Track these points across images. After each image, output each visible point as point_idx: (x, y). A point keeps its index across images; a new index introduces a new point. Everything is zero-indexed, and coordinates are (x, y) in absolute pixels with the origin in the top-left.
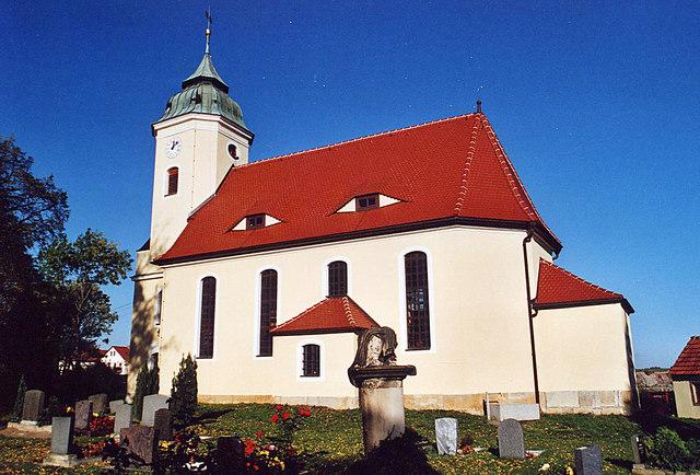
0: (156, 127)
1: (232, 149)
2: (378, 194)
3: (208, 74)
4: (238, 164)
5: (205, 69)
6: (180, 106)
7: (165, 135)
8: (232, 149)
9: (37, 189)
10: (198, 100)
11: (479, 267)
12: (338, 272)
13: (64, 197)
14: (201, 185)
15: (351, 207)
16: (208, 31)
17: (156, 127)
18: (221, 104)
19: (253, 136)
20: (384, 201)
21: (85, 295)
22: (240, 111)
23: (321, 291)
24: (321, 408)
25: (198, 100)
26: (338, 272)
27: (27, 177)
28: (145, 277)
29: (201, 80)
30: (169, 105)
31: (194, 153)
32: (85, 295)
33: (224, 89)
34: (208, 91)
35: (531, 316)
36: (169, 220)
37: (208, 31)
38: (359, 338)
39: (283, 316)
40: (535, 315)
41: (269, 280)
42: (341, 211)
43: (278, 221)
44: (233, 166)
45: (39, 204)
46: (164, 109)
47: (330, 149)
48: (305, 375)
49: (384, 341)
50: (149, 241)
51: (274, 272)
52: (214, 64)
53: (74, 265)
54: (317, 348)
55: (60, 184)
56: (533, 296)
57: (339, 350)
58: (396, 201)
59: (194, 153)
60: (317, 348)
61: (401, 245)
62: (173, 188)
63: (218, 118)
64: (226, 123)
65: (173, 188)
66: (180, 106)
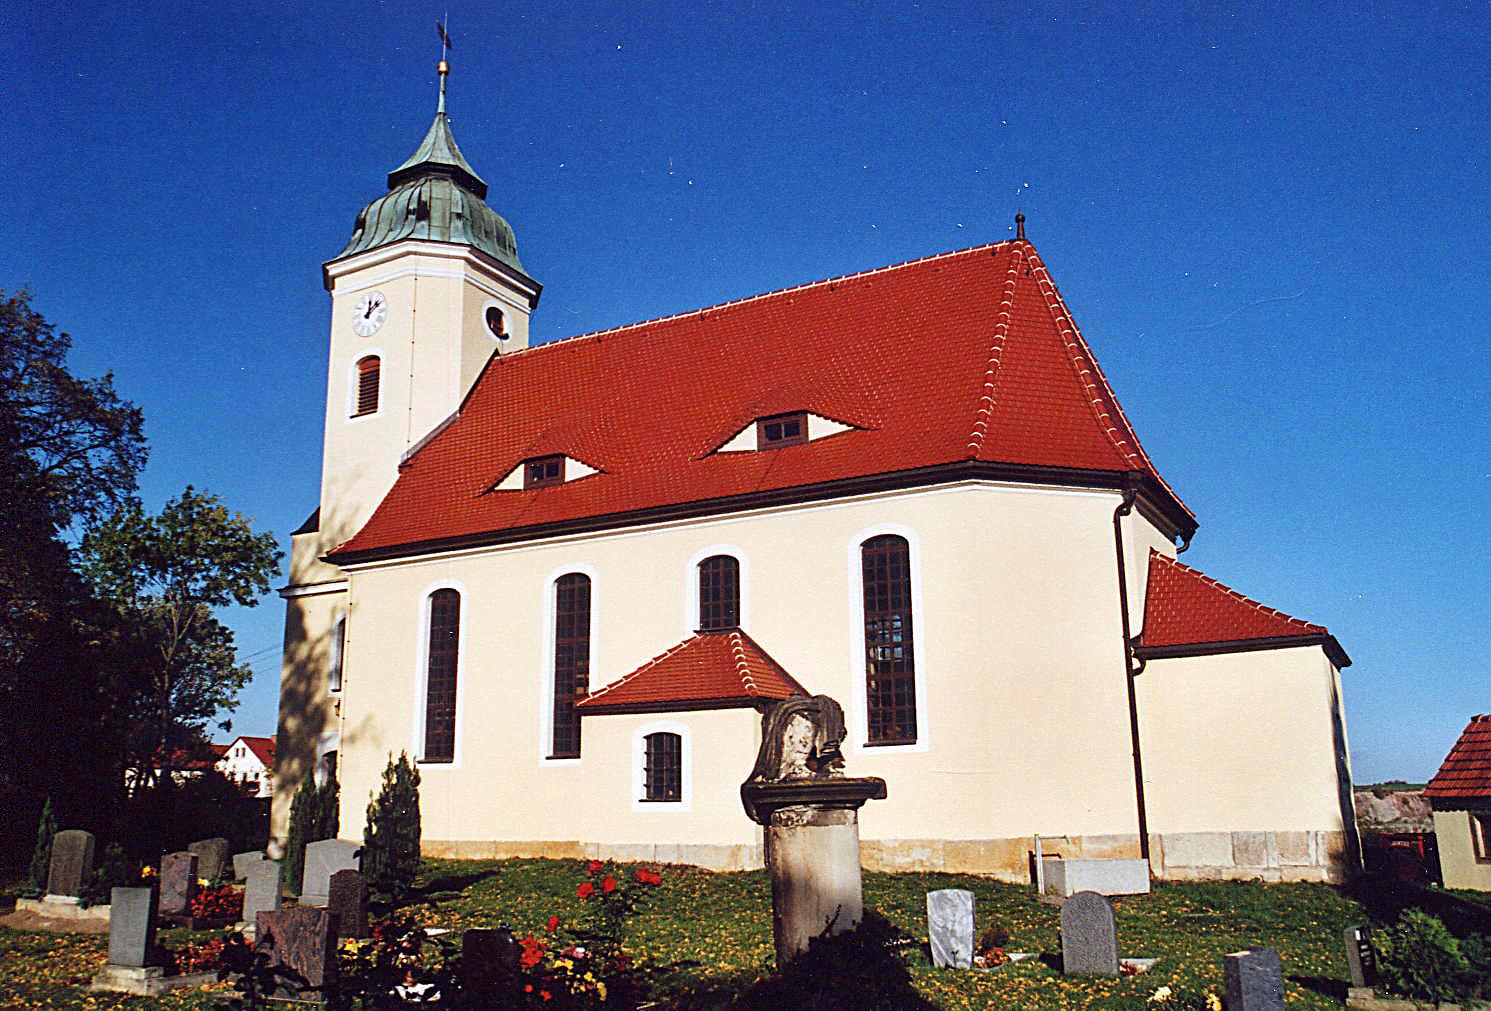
0: (333, 270)
1: (494, 317)
3: (444, 157)
4: (509, 348)
5: (436, 146)
6: (384, 227)
7: (352, 287)
8: (494, 317)
9: (80, 402)
10: (423, 212)
11: (1021, 573)
12: (720, 581)
13: (136, 418)
14: (428, 393)
15: (748, 440)
16: (443, 67)
17: (333, 270)
18: (471, 221)
20: (819, 428)
21: (181, 628)
22: (512, 237)
25: (423, 212)
26: (720, 581)
27: (59, 377)
28: (310, 590)
29: (428, 170)
30: (361, 224)
32: (181, 628)
33: (480, 191)
34: (444, 195)
35: (1132, 674)
37: (443, 67)
40: (1140, 671)
42: (726, 448)
44: (496, 353)
46: (347, 232)
55: (126, 393)
56: (1135, 630)
57: (722, 745)
58: (844, 428)
59: (414, 327)
61: (843, 527)
62: (368, 400)
63: (465, 252)
64: (482, 261)
65: (368, 400)
66: (384, 227)
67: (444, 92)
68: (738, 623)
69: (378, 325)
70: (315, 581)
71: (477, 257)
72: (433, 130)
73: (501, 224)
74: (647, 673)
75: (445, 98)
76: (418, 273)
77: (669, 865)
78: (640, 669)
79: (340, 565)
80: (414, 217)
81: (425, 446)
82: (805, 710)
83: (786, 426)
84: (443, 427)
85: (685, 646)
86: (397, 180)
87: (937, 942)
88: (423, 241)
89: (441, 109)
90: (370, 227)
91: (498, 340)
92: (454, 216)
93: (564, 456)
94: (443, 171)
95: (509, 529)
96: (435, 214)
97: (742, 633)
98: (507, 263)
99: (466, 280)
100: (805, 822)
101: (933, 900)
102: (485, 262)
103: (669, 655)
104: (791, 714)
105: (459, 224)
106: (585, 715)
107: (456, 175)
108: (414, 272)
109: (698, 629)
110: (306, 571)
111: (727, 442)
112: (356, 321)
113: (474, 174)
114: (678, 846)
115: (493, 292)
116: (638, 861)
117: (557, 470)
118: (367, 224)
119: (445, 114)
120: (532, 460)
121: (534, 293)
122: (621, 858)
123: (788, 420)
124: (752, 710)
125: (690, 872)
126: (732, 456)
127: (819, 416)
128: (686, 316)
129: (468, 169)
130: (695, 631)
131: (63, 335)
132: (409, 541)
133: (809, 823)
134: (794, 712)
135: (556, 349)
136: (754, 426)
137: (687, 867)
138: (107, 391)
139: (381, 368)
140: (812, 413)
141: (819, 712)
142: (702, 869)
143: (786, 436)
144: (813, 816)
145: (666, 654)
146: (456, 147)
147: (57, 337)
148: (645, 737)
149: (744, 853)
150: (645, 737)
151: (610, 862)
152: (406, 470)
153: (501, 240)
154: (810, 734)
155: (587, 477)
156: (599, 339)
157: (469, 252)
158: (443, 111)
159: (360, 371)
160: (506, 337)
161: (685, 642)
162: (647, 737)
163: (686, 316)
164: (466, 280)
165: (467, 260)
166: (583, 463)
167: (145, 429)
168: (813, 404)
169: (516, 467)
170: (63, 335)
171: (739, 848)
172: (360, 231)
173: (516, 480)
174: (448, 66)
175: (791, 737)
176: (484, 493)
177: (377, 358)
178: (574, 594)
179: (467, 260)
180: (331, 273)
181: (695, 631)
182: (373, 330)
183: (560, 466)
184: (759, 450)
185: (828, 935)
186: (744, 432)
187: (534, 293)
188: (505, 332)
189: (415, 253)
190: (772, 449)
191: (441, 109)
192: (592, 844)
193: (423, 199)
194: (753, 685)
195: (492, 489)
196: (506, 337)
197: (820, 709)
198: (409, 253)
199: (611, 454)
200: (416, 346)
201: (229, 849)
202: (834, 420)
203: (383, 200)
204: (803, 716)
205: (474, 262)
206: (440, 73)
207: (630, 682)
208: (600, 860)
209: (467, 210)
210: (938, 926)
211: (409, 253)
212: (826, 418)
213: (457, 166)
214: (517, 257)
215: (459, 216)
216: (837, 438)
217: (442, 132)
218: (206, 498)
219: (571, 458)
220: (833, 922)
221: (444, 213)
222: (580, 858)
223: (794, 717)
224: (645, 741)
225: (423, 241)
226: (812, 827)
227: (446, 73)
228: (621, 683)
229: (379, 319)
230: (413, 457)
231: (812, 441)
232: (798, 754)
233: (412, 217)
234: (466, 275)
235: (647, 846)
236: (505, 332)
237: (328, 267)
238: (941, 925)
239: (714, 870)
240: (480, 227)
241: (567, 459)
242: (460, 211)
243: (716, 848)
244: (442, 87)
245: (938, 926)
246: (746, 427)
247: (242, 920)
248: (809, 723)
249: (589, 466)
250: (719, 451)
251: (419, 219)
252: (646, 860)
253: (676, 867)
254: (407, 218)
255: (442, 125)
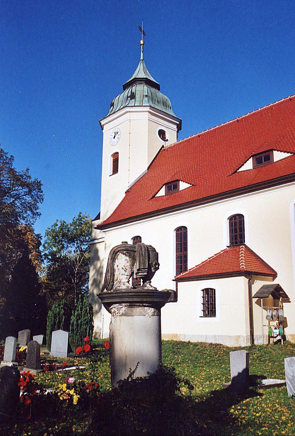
0: (103, 123)
1: (162, 134)
2: (272, 150)
4: (167, 144)
5: (140, 72)
6: (120, 104)
7: (109, 127)
8: (162, 134)
9: (19, 180)
10: (133, 96)
12: (237, 224)
13: (38, 185)
14: (136, 165)
15: (249, 165)
16: (142, 42)
17: (103, 123)
18: (151, 98)
19: (180, 121)
20: (278, 156)
21: (80, 261)
22: (169, 103)
23: (222, 241)
24: (217, 345)
25: (133, 96)
26: (237, 224)
27: (12, 171)
28: (100, 240)
29: (136, 81)
30: (112, 105)
31: (133, 138)
32: (80, 261)
33: (156, 86)
34: (140, 89)
36: (113, 193)
37: (142, 42)
38: (249, 281)
39: (192, 263)
41: (182, 234)
42: (240, 170)
43: (189, 185)
44: (163, 147)
45: (22, 191)
46: (107, 108)
47: (238, 121)
48: (205, 316)
49: (133, 260)
50: (100, 213)
51: (185, 228)
52: (149, 67)
53: (72, 240)
54: (213, 291)
55: (34, 176)
57: (232, 292)
58: (289, 155)
59: (133, 138)
60: (213, 291)
62: (115, 170)
63: (148, 109)
64: (155, 112)
65: (115, 170)
66: (120, 104)
67: (142, 52)
68: (244, 242)
69: (118, 140)
70: (102, 237)
71: (152, 110)
72: (139, 66)
73: (165, 98)
74: (204, 264)
75: (143, 54)
76: (131, 119)
77: (211, 344)
78: (202, 262)
79: (101, 230)
80: (130, 99)
81: (135, 184)
82: (125, 250)
83: (264, 157)
84: (141, 176)
85: (222, 252)
86: (125, 87)
87: (289, 383)
88: (132, 106)
89: (142, 58)
90: (116, 105)
91: (163, 142)
92: (145, 96)
93: (179, 180)
94: (142, 81)
95: (156, 210)
96: (137, 96)
97: (246, 246)
98: (166, 112)
99: (149, 120)
100: (121, 314)
101: (287, 362)
102: (165, 116)
103: (215, 256)
104: (117, 252)
105: (146, 99)
106: (179, 282)
107: (147, 82)
108: (129, 119)
109: (229, 245)
110: (98, 234)
111: (240, 167)
112: (111, 140)
113: (154, 81)
114: (215, 336)
115: (161, 124)
116: (200, 342)
117: (176, 187)
118: (114, 105)
119: (143, 60)
120: (168, 183)
121: (178, 123)
122: (193, 341)
123: (264, 154)
124: (243, 277)
125: (219, 347)
126: (240, 173)
127: (278, 151)
128: (232, 121)
129: (152, 79)
130: (227, 247)
131: (11, 156)
132: (123, 219)
133: (123, 315)
134: (118, 251)
135: (184, 142)
136: (251, 159)
137: (218, 345)
138: (27, 175)
139: (119, 157)
140: (275, 150)
141: (135, 252)
142: (224, 346)
143: (264, 161)
144: (125, 311)
145: (214, 256)
146: (148, 71)
147: (9, 157)
148: (201, 290)
149: (241, 339)
150: (201, 290)
151: (189, 342)
152: (128, 193)
153: (165, 104)
154: (128, 264)
155: (188, 188)
156: (199, 136)
157: (150, 109)
158: (142, 59)
159: (113, 159)
160: (167, 140)
161: (222, 251)
162: (203, 290)
163: (232, 121)
164: (149, 120)
165: (149, 112)
166: (186, 183)
167: (42, 188)
168: (276, 146)
169: (162, 187)
170: (11, 156)
171: (239, 337)
172: (112, 107)
173: (162, 192)
174: (144, 42)
175: (117, 266)
176: (151, 198)
177: (118, 153)
178: (182, 234)
179: (149, 112)
180: (102, 124)
181: (227, 247)
182: (116, 143)
183: (178, 185)
184: (253, 169)
185: (130, 380)
186: (247, 162)
187: (178, 123)
188: (166, 139)
189: (129, 112)
190: (259, 167)
191: (142, 58)
192: (182, 334)
193: (133, 91)
194: (244, 266)
195: (236, 172)
196: (167, 140)
197: (136, 250)
198: (127, 112)
199: (197, 178)
200: (129, 144)
201: (31, 334)
202: (285, 152)
203: (119, 95)
204: (124, 254)
205: (152, 112)
206: (141, 45)
207: (198, 268)
208: (186, 341)
209: (150, 94)
210: (290, 376)
211: (127, 112)
212: (281, 151)
213: (146, 78)
214: (172, 110)
215: (146, 96)
216: (286, 159)
217: (142, 67)
218: (86, 216)
219: (182, 181)
220: (134, 372)
221: (141, 94)
222: (178, 340)
223: (118, 254)
224: (202, 292)
225: (132, 106)
226: (124, 317)
227: (143, 44)
228: (195, 268)
229: (118, 138)
230: (130, 188)
231: (275, 162)
232: (123, 276)
233: (129, 99)
234: (149, 118)
235: (202, 336)
236: (166, 139)
237: (101, 122)
238: (292, 375)
239: (229, 346)
240: (156, 100)
241: (180, 181)
242: (147, 94)
243: (230, 337)
244: (142, 50)
245: (290, 376)
246: (248, 160)
247: (3, 360)
248: (127, 258)
249: (188, 183)
250: (238, 171)
251: (131, 99)
252: (202, 341)
253: (214, 345)
254: (127, 99)
255: (142, 64)
